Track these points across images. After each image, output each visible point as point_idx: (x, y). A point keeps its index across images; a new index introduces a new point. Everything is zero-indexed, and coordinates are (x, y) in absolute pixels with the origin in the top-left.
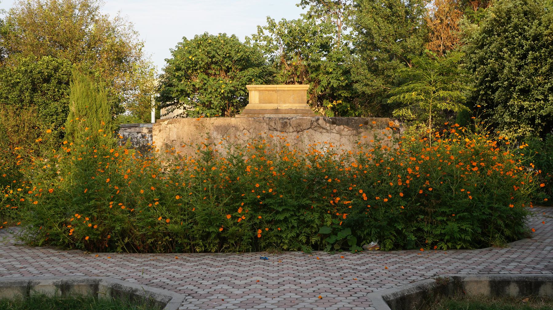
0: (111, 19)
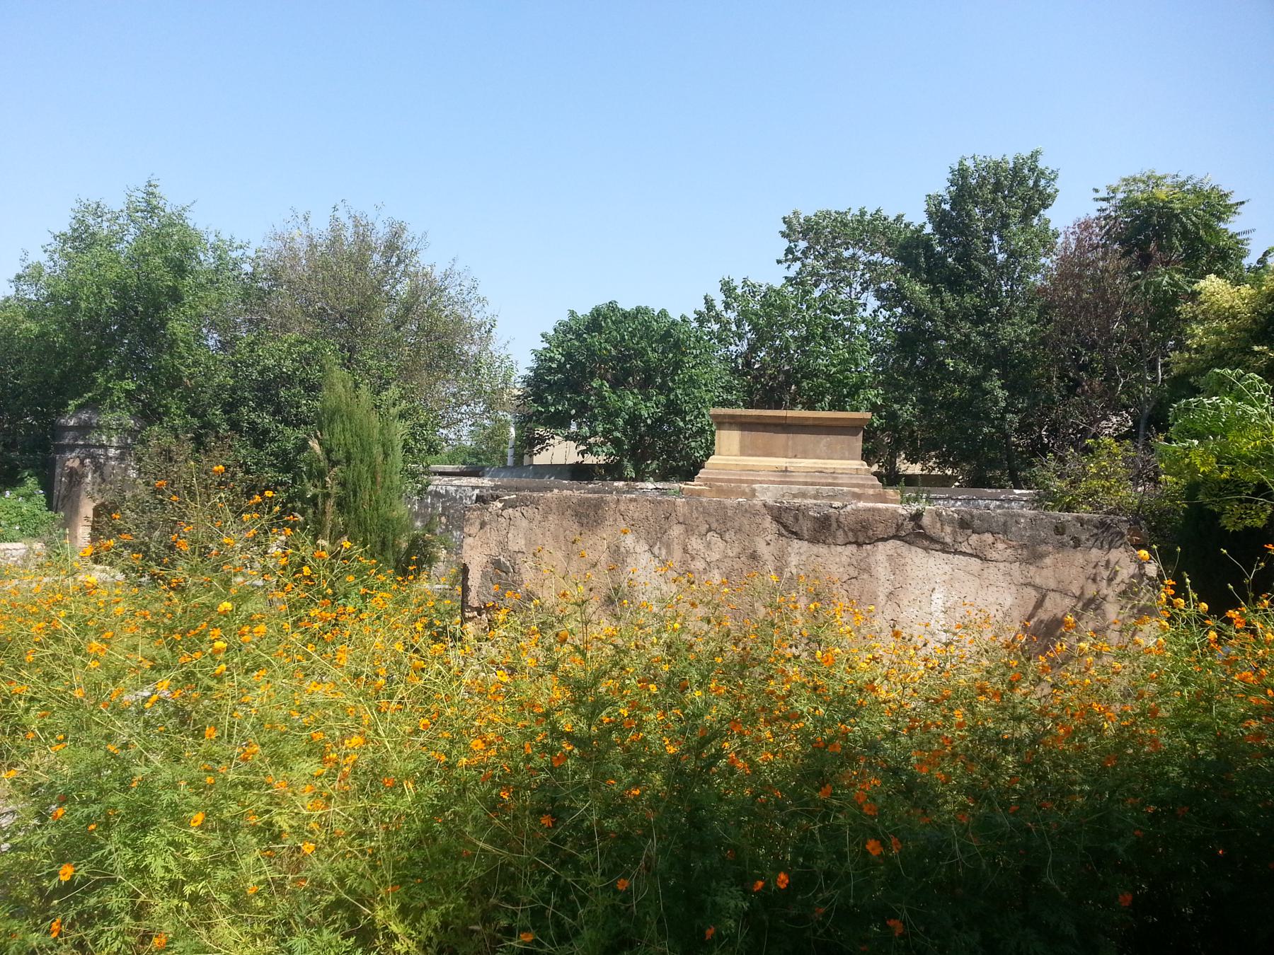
0: (437, 273)
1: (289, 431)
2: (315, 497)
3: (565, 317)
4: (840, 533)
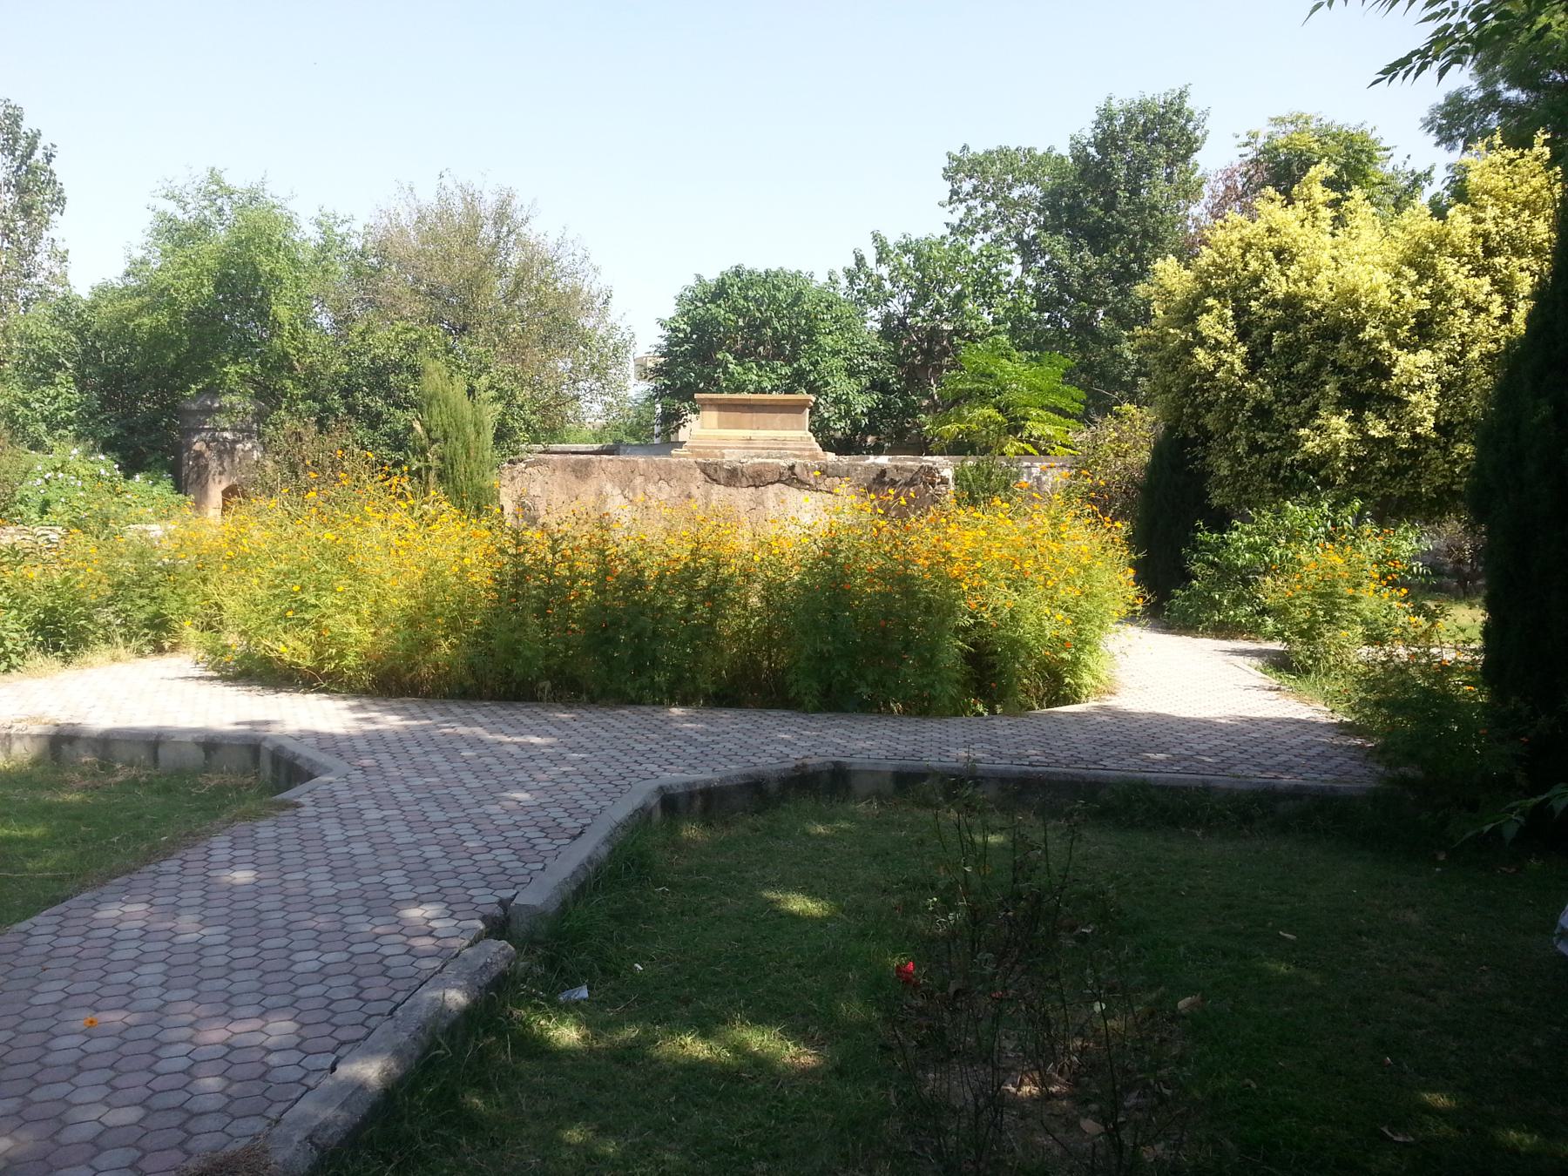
0: (551, 242)
1: (399, 413)
2: (419, 469)
3: (692, 282)
4: (744, 479)
